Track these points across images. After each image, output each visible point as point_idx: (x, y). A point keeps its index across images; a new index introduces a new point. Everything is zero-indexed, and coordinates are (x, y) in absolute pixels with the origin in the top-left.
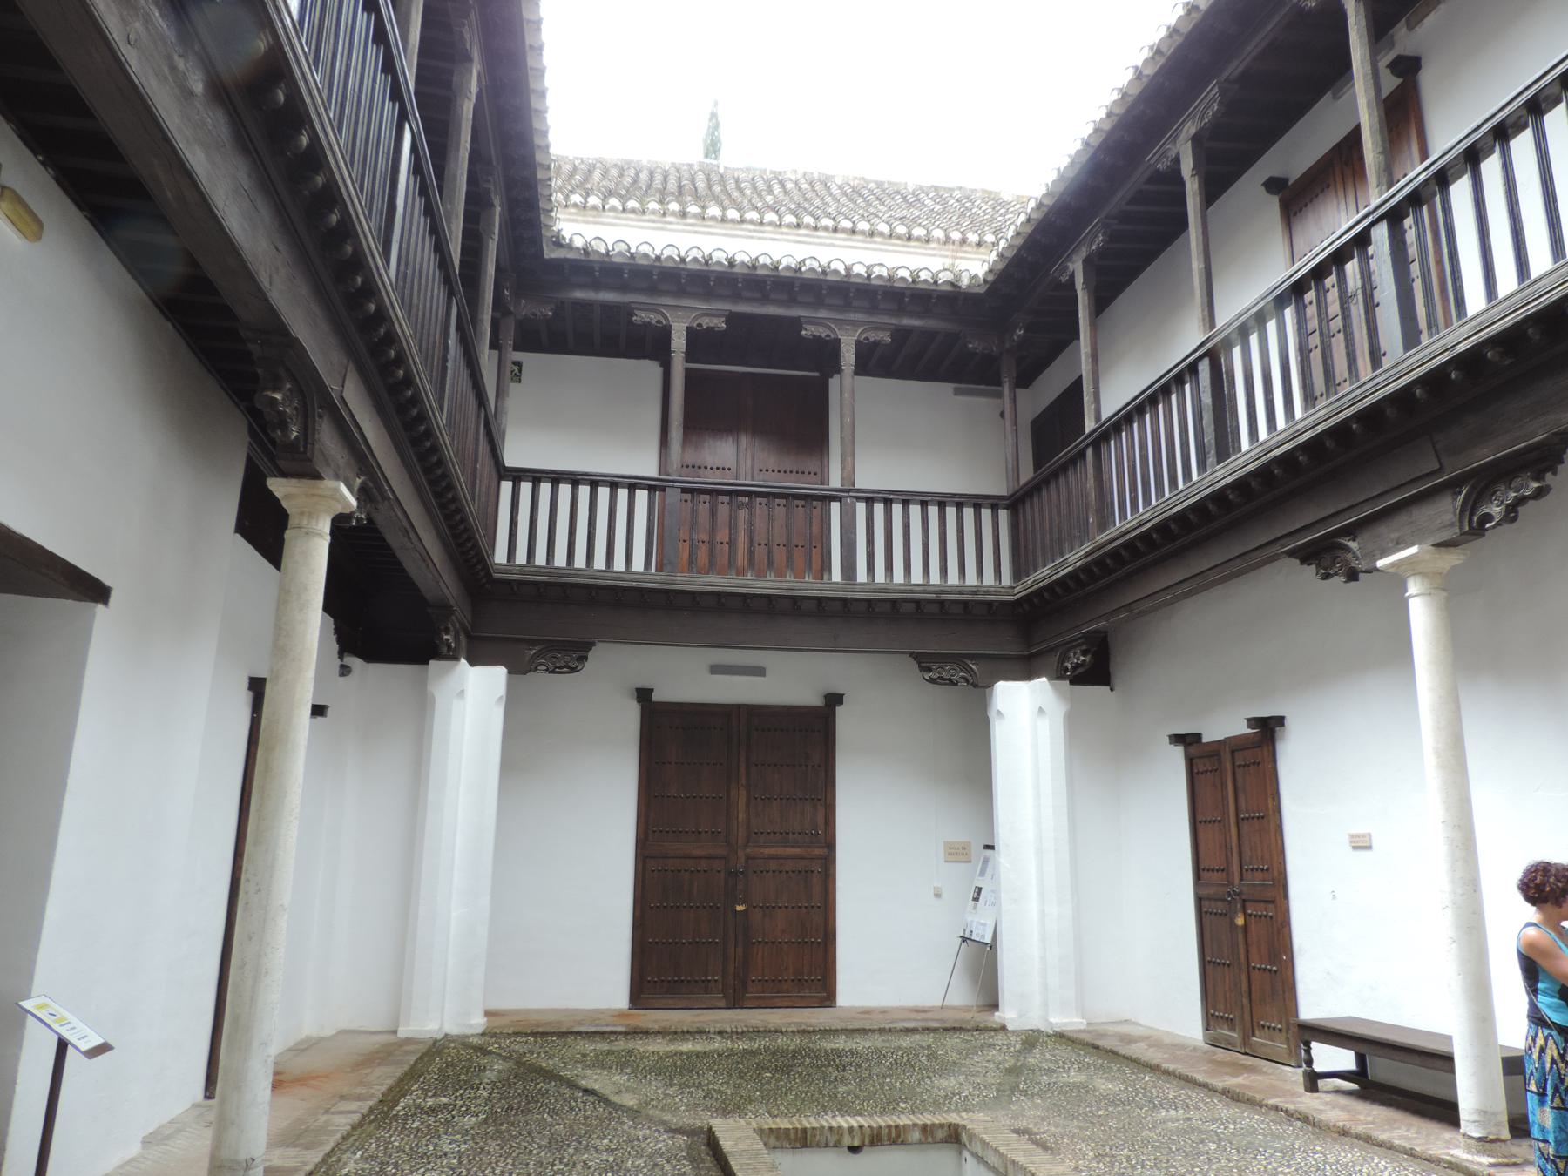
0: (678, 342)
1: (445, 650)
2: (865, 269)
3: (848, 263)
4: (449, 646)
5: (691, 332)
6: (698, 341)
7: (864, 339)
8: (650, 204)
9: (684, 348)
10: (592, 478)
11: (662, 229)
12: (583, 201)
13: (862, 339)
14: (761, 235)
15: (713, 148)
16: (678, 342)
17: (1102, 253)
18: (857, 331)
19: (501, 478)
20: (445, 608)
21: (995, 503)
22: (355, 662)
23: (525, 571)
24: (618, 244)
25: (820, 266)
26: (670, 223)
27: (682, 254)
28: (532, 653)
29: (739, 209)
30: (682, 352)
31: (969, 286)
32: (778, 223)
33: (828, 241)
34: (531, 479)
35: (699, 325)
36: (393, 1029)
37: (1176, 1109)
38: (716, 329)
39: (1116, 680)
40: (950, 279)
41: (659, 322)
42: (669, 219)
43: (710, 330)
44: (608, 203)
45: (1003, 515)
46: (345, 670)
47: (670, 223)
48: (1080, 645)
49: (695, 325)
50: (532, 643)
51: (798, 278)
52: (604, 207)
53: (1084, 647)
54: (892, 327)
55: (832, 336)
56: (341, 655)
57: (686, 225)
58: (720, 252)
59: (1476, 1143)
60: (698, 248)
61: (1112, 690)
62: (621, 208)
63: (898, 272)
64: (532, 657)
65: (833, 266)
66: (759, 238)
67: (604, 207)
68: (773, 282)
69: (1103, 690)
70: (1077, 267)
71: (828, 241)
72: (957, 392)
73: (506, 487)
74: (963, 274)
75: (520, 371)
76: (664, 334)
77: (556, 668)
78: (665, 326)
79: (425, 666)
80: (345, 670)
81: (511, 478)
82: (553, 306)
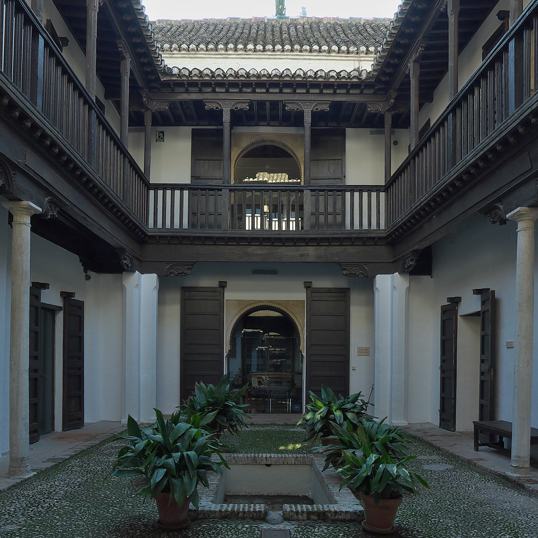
0: (308, 119)
1: (126, 267)
2: (314, 73)
3: (305, 71)
4: (127, 266)
5: (313, 114)
6: (316, 116)
7: (235, 108)
8: (219, 46)
9: (229, 121)
10: (189, 186)
11: (226, 58)
12: (187, 47)
13: (234, 108)
14: (274, 57)
15: (280, 12)
16: (308, 119)
17: (423, 57)
18: (312, 105)
19: (149, 189)
20: (123, 250)
21: (377, 189)
22: (91, 273)
23: (160, 231)
24: (194, 70)
25: (291, 74)
26: (231, 54)
27: (270, 73)
28: (168, 267)
29: (338, 45)
30: (228, 123)
31: (366, 79)
32: (282, 50)
33: (308, 57)
34: (187, 189)
35: (236, 108)
36: (120, 420)
37: (266, 458)
38: (325, 110)
39: (434, 273)
40: (356, 75)
41: (217, 108)
42: (362, 55)
43: (322, 111)
44: (199, 47)
45: (382, 195)
46: (88, 278)
47: (231, 54)
48: (409, 257)
49: (234, 108)
50: (168, 263)
51: (281, 81)
52: (197, 49)
53: (411, 258)
54: (249, 101)
55: (220, 108)
56: (85, 271)
57: (237, 55)
58: (242, 70)
59: (514, 469)
60: (232, 69)
61: (432, 277)
62: (205, 49)
63: (330, 74)
64: (168, 270)
65: (298, 73)
66: (274, 59)
67: (197, 49)
68: (229, 83)
69: (426, 278)
70: (411, 65)
71: (308, 57)
72: (372, 133)
73: (152, 192)
74: (363, 72)
75: (163, 136)
76: (220, 113)
77: (178, 274)
78: (221, 109)
79: (121, 274)
80: (88, 278)
81: (187, 189)
82: (168, 104)
